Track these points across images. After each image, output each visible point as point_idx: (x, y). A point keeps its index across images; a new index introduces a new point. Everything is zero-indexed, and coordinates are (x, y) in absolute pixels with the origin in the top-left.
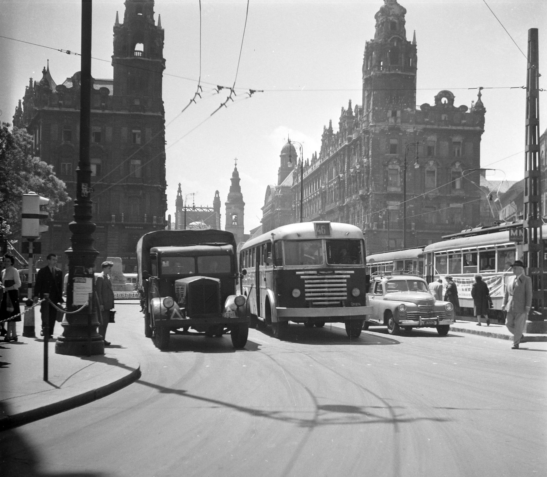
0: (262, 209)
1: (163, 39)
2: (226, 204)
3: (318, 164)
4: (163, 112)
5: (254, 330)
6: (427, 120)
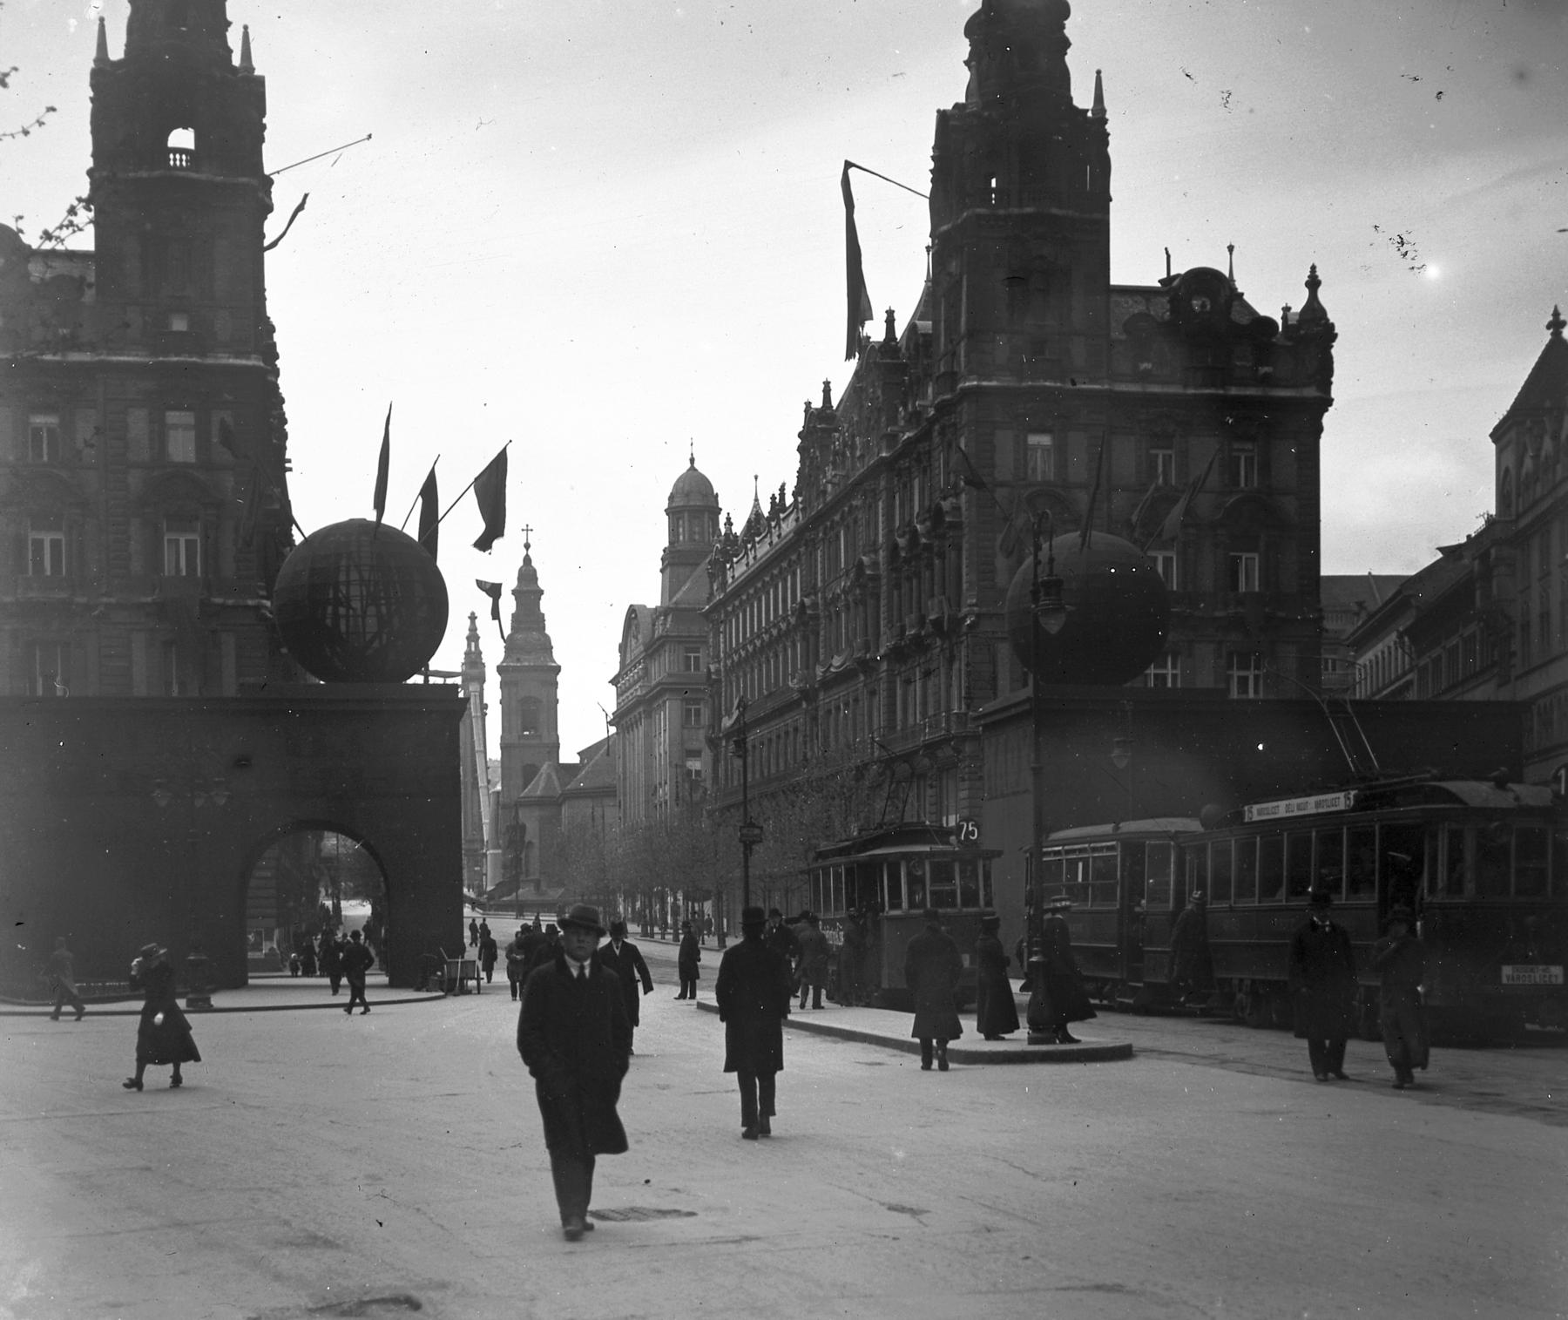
0: (614, 681)
1: (262, 112)
2: (514, 592)
3: (788, 526)
4: (271, 354)
5: (297, 486)
6: (1145, 366)
